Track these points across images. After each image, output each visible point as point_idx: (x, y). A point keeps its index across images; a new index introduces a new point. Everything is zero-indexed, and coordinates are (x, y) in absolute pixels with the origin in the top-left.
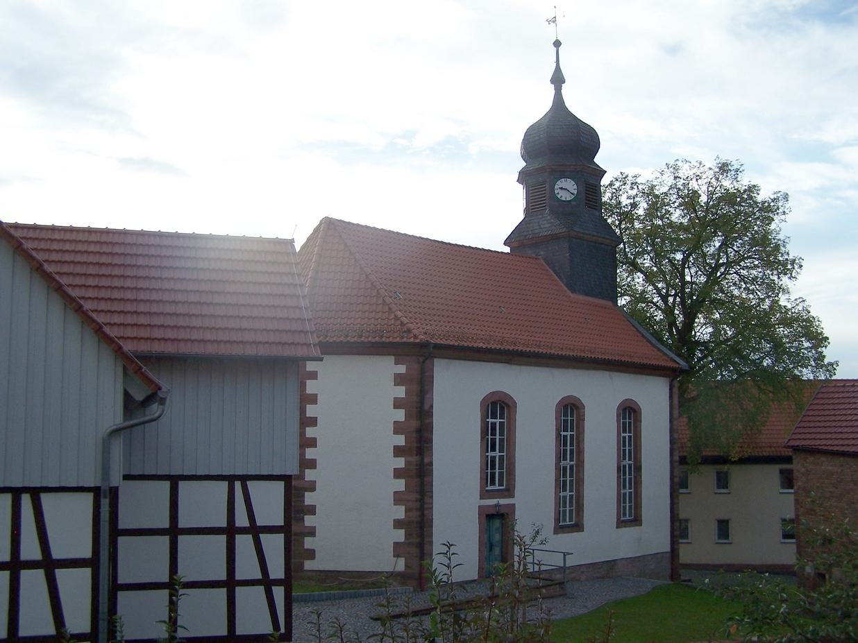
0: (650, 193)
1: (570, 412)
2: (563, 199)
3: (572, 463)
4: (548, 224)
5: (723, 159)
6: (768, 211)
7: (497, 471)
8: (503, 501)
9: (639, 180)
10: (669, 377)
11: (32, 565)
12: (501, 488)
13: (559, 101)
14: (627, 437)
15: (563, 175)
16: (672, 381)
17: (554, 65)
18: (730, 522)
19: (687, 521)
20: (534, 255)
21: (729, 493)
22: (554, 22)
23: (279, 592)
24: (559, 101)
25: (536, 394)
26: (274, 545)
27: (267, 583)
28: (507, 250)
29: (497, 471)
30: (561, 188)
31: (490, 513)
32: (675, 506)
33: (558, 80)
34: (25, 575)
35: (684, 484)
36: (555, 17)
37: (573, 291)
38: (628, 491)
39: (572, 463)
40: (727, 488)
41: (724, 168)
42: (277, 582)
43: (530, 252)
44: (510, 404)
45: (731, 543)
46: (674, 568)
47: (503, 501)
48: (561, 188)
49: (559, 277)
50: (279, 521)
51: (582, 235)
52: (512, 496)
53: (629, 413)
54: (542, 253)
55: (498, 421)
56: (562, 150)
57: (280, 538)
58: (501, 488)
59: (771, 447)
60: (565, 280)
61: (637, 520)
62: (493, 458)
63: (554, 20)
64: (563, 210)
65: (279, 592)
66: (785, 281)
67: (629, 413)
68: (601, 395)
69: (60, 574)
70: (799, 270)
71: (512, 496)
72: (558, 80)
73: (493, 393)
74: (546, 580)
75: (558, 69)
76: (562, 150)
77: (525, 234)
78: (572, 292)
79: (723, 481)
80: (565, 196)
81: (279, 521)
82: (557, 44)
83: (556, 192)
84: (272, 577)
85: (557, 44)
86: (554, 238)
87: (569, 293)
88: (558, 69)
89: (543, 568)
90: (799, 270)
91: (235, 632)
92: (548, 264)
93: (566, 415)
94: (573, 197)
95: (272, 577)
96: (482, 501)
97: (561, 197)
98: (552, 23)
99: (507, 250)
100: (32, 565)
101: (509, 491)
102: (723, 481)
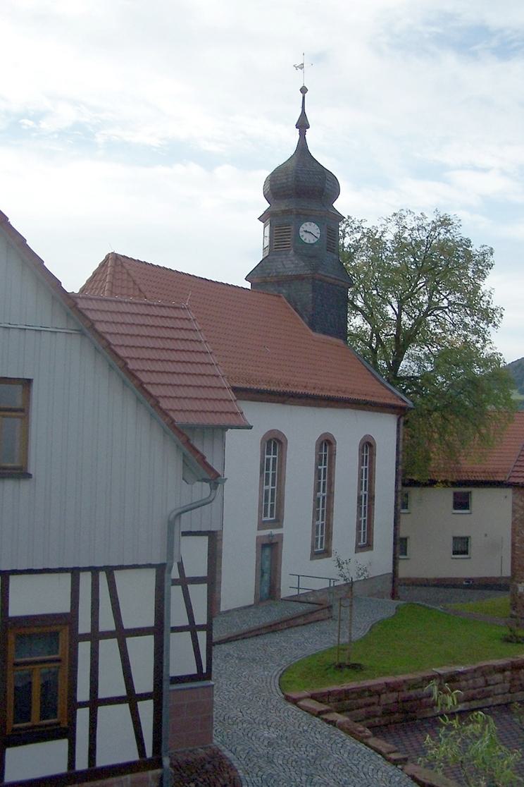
0: (369, 235)
1: (326, 444)
2: (307, 241)
3: (324, 494)
4: (290, 265)
5: (451, 214)
6: (482, 265)
7: (272, 507)
8: (275, 532)
9: (363, 225)
10: (397, 414)
11: (107, 635)
12: (272, 519)
13: (302, 147)
14: (271, 459)
15: (308, 218)
16: (400, 417)
17: (301, 110)
18: (408, 540)
19: (406, 539)
20: (276, 293)
21: (471, 513)
22: (301, 68)
23: (202, 636)
24: (302, 147)
25: (302, 428)
26: (199, 593)
27: (192, 628)
28: (248, 285)
29: (272, 507)
30: (306, 231)
31: (264, 543)
32: (398, 527)
33: (303, 125)
34: (103, 644)
35: (405, 506)
36: (303, 64)
37: (314, 330)
38: (362, 519)
39: (324, 494)
40: (407, 508)
41: (445, 222)
42: (201, 628)
43: (272, 289)
44: (283, 441)
45: (470, 558)
46: (396, 584)
47: (275, 532)
48: (306, 231)
49: (301, 315)
50: (203, 572)
51: (323, 277)
52: (281, 526)
53: (368, 446)
54: (284, 291)
55: (272, 456)
56: (301, 191)
57: (204, 587)
58: (272, 519)
59: (472, 472)
60: (307, 319)
61: (369, 545)
62: (267, 492)
63: (302, 66)
64: (307, 253)
65: (202, 636)
66: (490, 328)
67: (368, 446)
68: (349, 429)
69: (130, 641)
70: (500, 319)
71: (281, 526)
72: (303, 125)
73: (271, 431)
74: (314, 603)
75: (303, 114)
76: (301, 191)
77: (268, 271)
78: (313, 331)
79: (462, 503)
80: (308, 239)
81: (203, 572)
82: (304, 90)
83: (301, 234)
84: (197, 623)
85: (304, 90)
86: (300, 278)
87: (310, 331)
88: (303, 114)
89: (301, 592)
90: (500, 319)
91: (194, 675)
92: (289, 302)
93: (321, 451)
94: (316, 240)
95: (197, 623)
96: (259, 532)
97: (305, 239)
98: (299, 70)
99: (248, 285)
100: (107, 635)
101: (278, 522)
102: (462, 503)
